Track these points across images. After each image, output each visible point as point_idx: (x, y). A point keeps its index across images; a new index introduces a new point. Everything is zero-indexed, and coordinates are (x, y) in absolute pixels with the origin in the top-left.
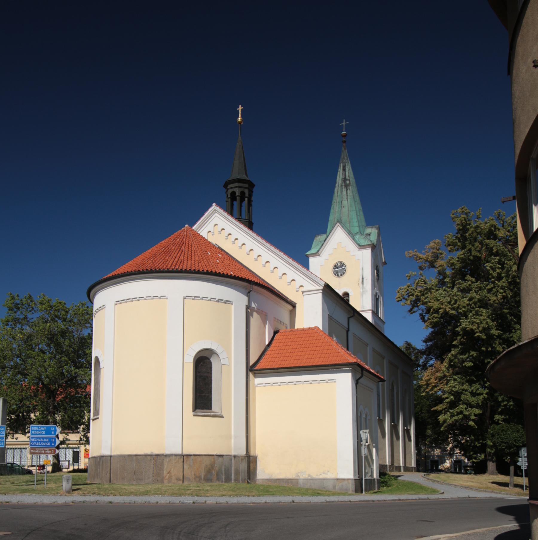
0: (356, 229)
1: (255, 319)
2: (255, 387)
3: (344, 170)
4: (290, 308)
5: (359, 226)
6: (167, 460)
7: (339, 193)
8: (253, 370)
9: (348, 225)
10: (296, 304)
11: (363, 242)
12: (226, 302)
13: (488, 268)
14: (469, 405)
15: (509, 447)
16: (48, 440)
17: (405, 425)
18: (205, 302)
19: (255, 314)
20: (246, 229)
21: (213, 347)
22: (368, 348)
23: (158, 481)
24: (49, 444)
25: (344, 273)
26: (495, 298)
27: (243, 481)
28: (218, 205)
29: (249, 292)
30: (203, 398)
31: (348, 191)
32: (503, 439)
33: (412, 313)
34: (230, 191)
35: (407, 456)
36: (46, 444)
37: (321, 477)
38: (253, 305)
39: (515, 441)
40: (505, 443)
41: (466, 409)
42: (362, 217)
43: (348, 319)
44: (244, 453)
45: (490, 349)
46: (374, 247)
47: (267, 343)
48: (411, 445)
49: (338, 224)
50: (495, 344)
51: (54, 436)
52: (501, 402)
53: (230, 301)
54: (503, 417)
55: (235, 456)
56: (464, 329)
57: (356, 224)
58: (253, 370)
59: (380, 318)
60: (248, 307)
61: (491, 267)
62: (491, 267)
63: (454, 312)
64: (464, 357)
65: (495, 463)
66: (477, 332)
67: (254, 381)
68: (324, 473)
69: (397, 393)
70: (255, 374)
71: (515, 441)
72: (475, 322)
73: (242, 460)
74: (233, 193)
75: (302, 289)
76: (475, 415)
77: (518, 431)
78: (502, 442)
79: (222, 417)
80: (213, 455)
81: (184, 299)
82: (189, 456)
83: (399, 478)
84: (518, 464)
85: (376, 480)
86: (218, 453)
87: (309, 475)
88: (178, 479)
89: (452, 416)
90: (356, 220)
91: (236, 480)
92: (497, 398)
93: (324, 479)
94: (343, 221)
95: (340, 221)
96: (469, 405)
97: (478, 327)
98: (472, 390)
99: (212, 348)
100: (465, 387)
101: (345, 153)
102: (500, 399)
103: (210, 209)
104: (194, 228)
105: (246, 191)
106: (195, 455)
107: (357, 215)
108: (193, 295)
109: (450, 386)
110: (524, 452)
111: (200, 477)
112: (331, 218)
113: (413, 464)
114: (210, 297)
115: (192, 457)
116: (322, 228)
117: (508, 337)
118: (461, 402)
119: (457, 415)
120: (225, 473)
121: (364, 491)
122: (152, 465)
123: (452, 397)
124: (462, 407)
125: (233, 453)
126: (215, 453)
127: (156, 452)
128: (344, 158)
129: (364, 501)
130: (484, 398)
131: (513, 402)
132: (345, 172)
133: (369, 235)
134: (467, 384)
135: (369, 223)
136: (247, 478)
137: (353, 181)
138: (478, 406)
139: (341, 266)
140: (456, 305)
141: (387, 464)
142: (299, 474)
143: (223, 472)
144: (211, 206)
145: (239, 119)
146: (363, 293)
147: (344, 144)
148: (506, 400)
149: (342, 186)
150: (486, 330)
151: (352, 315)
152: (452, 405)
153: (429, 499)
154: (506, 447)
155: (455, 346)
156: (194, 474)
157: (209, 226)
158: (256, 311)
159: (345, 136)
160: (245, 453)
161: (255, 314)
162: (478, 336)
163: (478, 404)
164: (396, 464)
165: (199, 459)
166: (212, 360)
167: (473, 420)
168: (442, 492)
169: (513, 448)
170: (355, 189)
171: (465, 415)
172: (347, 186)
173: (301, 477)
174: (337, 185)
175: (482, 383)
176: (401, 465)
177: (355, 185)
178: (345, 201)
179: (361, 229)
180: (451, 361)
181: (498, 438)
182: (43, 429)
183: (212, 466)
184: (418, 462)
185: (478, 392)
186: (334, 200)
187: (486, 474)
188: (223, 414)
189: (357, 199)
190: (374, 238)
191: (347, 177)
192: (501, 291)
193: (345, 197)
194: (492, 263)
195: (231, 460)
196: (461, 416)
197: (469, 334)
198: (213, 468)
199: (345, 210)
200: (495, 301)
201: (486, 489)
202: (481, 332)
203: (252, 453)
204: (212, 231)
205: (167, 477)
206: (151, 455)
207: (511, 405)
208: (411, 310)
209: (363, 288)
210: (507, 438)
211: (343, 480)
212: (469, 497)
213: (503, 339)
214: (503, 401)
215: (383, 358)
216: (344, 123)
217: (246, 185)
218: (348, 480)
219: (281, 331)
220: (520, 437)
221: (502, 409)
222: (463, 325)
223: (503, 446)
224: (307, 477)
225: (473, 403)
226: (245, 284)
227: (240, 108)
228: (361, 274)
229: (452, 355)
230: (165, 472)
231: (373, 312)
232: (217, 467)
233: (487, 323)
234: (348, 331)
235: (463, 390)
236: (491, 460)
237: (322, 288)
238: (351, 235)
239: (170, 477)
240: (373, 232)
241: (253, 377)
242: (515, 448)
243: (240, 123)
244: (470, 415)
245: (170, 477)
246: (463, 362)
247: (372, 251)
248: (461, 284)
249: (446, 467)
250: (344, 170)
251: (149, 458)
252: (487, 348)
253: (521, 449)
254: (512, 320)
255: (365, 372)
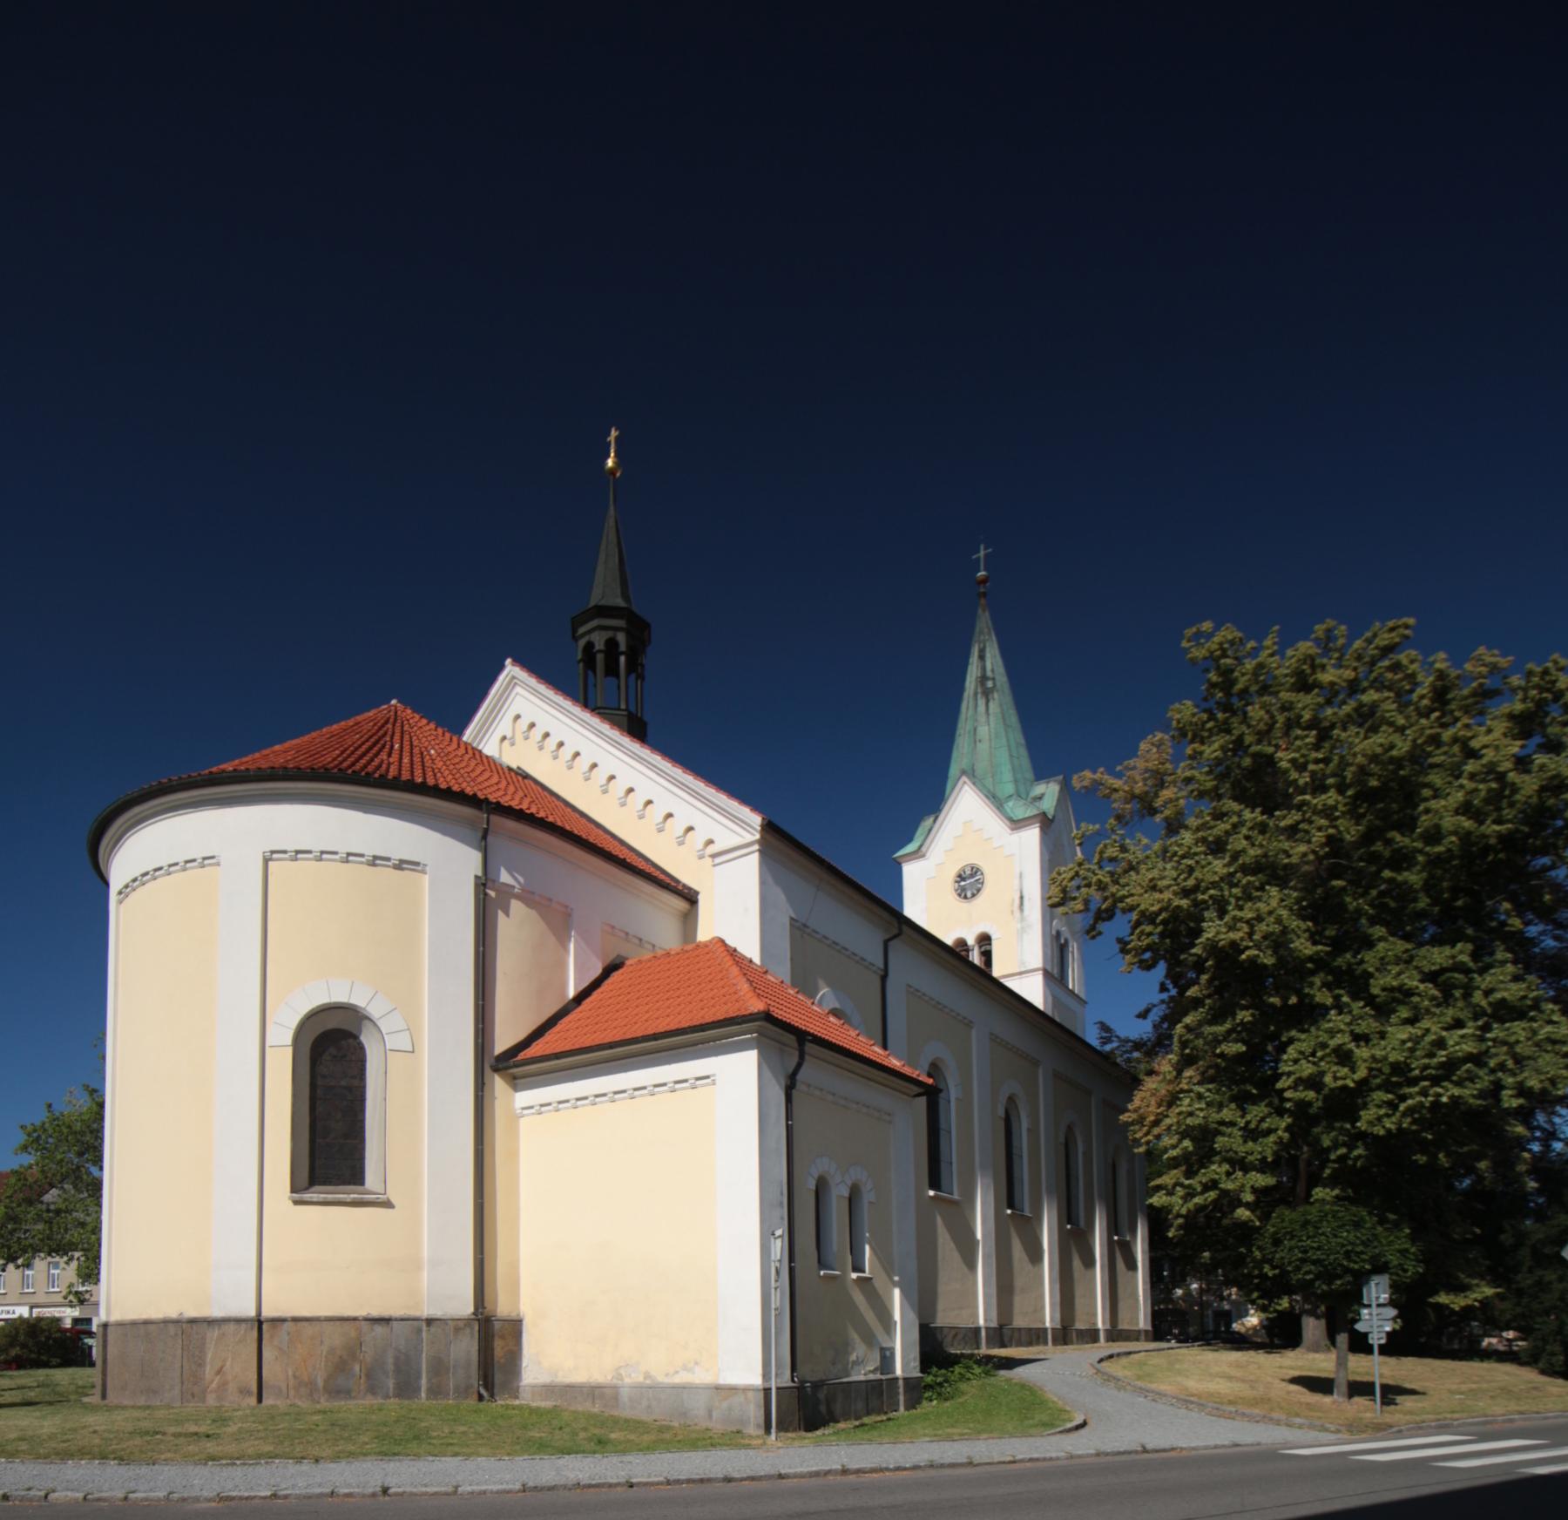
0: (1009, 788)
2: (514, 1119)
4: (681, 905)
5: (1016, 781)
6: (213, 1334)
7: (971, 712)
8: (502, 1065)
9: (989, 782)
10: (697, 893)
11: (1020, 810)
12: (401, 865)
13: (1284, 764)
15: (1328, 1275)
17: (1113, 1227)
18: (330, 867)
20: (626, 741)
22: (974, 1033)
23: (193, 1395)
25: (979, 890)
26: (1303, 848)
27: (462, 1392)
28: (519, 661)
29: (484, 837)
31: (991, 705)
32: (1305, 1252)
33: (1093, 937)
34: (582, 642)
35: (1122, 1306)
38: (505, 877)
39: (1347, 1255)
40: (1314, 1262)
41: (1228, 1174)
44: (467, 1309)
45: (1293, 1000)
46: (1046, 823)
48: (1136, 1279)
49: (964, 778)
50: (1311, 985)
52: (1329, 1150)
53: (417, 864)
54: (1336, 1192)
55: (430, 1321)
57: (1007, 776)
58: (502, 1065)
59: (1072, 992)
63: (1184, 903)
64: (1220, 1029)
65: (1323, 1322)
66: (1247, 948)
68: (685, 1368)
70: (515, 1078)
71: (1347, 1255)
72: (1240, 920)
73: (457, 1330)
75: (712, 849)
76: (1254, 1190)
77: (1357, 1225)
78: (1303, 1261)
79: (388, 1204)
80: (355, 1319)
81: (266, 861)
82: (278, 1321)
83: (1020, 1372)
84: (1360, 1327)
85: (901, 1383)
86: (375, 1313)
87: (647, 1375)
88: (243, 1391)
90: (1009, 767)
91: (436, 1392)
92: (1317, 1140)
94: (979, 772)
97: (1250, 934)
98: (1248, 1123)
99: (353, 1001)
100: (1227, 1114)
101: (984, 620)
102: (1326, 1142)
103: (501, 677)
104: (468, 736)
105: (621, 638)
106: (296, 1320)
107: (1011, 756)
108: (291, 846)
109: (1180, 1114)
112: (954, 770)
113: (1143, 1322)
115: (286, 1324)
116: (933, 801)
117: (1349, 965)
118: (1217, 1158)
119: (1202, 1193)
120: (398, 1370)
121: (773, 1430)
122: (179, 1352)
123: (1187, 1143)
124: (1217, 1169)
125: (426, 1311)
126: (362, 1313)
128: (981, 633)
130: (1280, 1142)
131: (1367, 1149)
132: (987, 660)
133: (1040, 798)
134: (1233, 1106)
135: (1041, 774)
136: (475, 1381)
137: (1002, 679)
138: (1263, 1167)
139: (972, 876)
141: (1048, 1324)
142: (622, 1372)
144: (501, 667)
145: (610, 463)
146: (1022, 931)
147: (983, 601)
148: (1344, 1144)
149: (976, 694)
150: (1278, 942)
151: (896, 931)
152: (1191, 1163)
154: (1318, 1277)
155: (1197, 1003)
156: (295, 1377)
157: (504, 726)
158: (518, 897)
159: (984, 581)
160: (472, 1309)
162: (1252, 961)
163: (1265, 1158)
164: (1080, 1325)
165: (308, 1329)
166: (363, 1038)
167: (1247, 1205)
168: (1078, 1421)
169: (1340, 1277)
170: (1009, 699)
171: (1225, 1193)
172: (987, 693)
173: (627, 1380)
174: (966, 695)
175: (1276, 1101)
176: (1100, 1325)
178: (986, 727)
179: (1022, 789)
181: (1291, 1249)
183: (353, 1350)
184: (1156, 1316)
185: (1265, 1125)
187: (1298, 1350)
188: (393, 1196)
189: (1014, 719)
191: (989, 674)
192: (1323, 822)
193: (982, 719)
194: (1298, 749)
195: (419, 1331)
196: (1212, 1195)
197: (1226, 956)
199: (983, 747)
200: (1305, 855)
201: (1258, 1407)
202: (1257, 946)
204: (509, 735)
205: (214, 1385)
206: (176, 1322)
207: (1359, 1157)
208: (1093, 928)
209: (1022, 919)
210: (1319, 1248)
211: (733, 1390)
212: (1145, 1450)
214: (1336, 1146)
215: (1036, 1063)
216: (982, 553)
217: (621, 623)
218: (746, 1389)
219: (628, 963)
220: (1363, 1243)
221: (1334, 1170)
223: (1307, 1273)
224: (641, 1379)
225: (1250, 1158)
227: (614, 433)
228: (1017, 887)
229: (1187, 1027)
230: (209, 1371)
231: (1047, 975)
233: (1279, 921)
234: (884, 978)
235: (1222, 1123)
236: (1313, 1313)
237: (758, 836)
240: (1049, 792)
241: (510, 1090)
242: (1349, 1278)
243: (612, 472)
244: (1242, 1189)
246: (1217, 1041)
248: (1211, 828)
249: (1249, 1325)
250: (982, 657)
251: (172, 1329)
252: (1285, 999)
253: (1367, 1282)
255: (809, 1047)
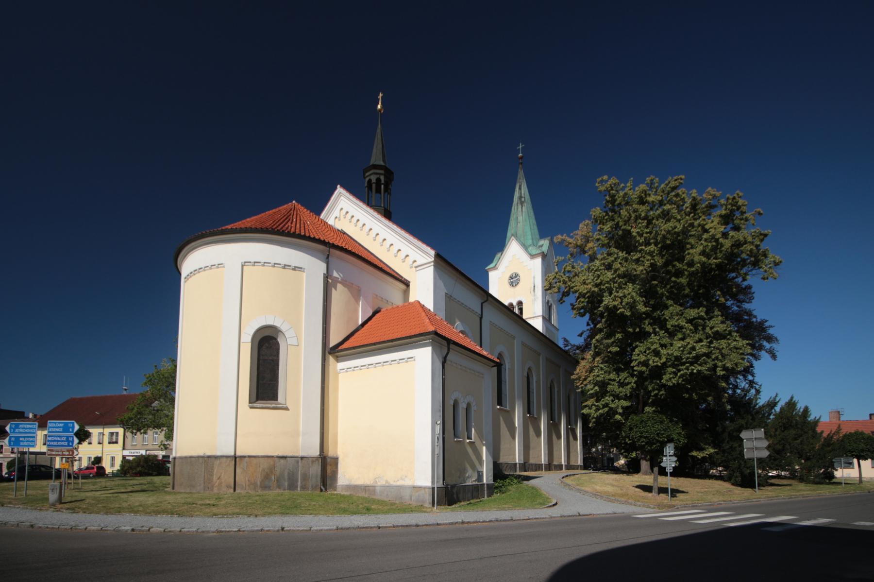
0: (530, 242)
1: (339, 294)
2: (337, 374)
3: (520, 189)
4: (403, 287)
8: (333, 351)
9: (522, 239)
11: (535, 251)
12: (295, 268)
13: (634, 234)
14: (617, 397)
15: (650, 443)
16: (65, 439)
17: (569, 422)
19: (339, 286)
21: (277, 324)
24: (66, 444)
26: (641, 268)
27: (314, 488)
28: (343, 186)
30: (265, 385)
34: (367, 179)
35: (571, 454)
36: (63, 443)
37: (398, 483)
38: (335, 274)
40: (645, 438)
41: (612, 401)
42: (536, 231)
43: (482, 304)
44: (316, 453)
45: (638, 330)
46: (544, 256)
47: (360, 323)
51: (72, 434)
52: (651, 392)
55: (302, 458)
56: (607, 308)
57: (529, 237)
58: (333, 351)
60: (327, 277)
61: (638, 233)
62: (638, 233)
63: (596, 289)
64: (610, 341)
65: (649, 463)
67: (336, 367)
68: (402, 479)
69: (559, 392)
70: (337, 357)
73: (313, 462)
74: (370, 181)
76: (622, 408)
77: (662, 422)
78: (641, 437)
79: (287, 409)
81: (243, 266)
84: (663, 465)
86: (281, 454)
88: (228, 487)
89: (597, 410)
91: (304, 488)
92: (647, 387)
93: (401, 487)
95: (515, 235)
96: (617, 397)
103: (336, 193)
104: (322, 216)
105: (382, 178)
106: (249, 457)
110: (669, 450)
111: (255, 484)
112: (509, 234)
113: (580, 462)
114: (273, 262)
116: (501, 247)
120: (289, 479)
124: (608, 399)
125: (301, 454)
126: (275, 454)
127: (209, 453)
129: (402, 526)
130: (632, 388)
133: (542, 246)
135: (542, 236)
138: (626, 398)
140: (599, 281)
143: (286, 477)
144: (336, 189)
145: (379, 107)
146: (534, 300)
150: (632, 306)
152: (599, 396)
153: (512, 520)
154: (647, 443)
157: (336, 213)
158: (340, 283)
159: (521, 158)
160: (318, 453)
161: (339, 286)
162: (622, 313)
165: (255, 461)
167: (620, 414)
170: (530, 206)
171: (611, 409)
172: (522, 203)
177: (529, 202)
180: (596, 347)
182: (62, 425)
183: (272, 469)
184: (585, 460)
186: (512, 218)
188: (289, 405)
189: (532, 214)
190: (545, 249)
192: (649, 258)
195: (298, 462)
196: (606, 409)
198: (272, 472)
199: (520, 225)
202: (624, 307)
203: (331, 453)
211: (420, 488)
212: (580, 515)
213: (654, 319)
214: (654, 390)
217: (382, 172)
218: (425, 488)
222: (605, 302)
226: (321, 247)
227: (381, 95)
230: (215, 478)
232: (278, 471)
233: (632, 297)
234: (481, 318)
235: (610, 380)
236: (645, 459)
238: (525, 247)
239: (220, 484)
240: (545, 243)
243: (380, 110)
245: (220, 484)
246: (608, 346)
247: (543, 259)
250: (520, 189)
252: (634, 330)
254: (662, 294)
255: (452, 346)
